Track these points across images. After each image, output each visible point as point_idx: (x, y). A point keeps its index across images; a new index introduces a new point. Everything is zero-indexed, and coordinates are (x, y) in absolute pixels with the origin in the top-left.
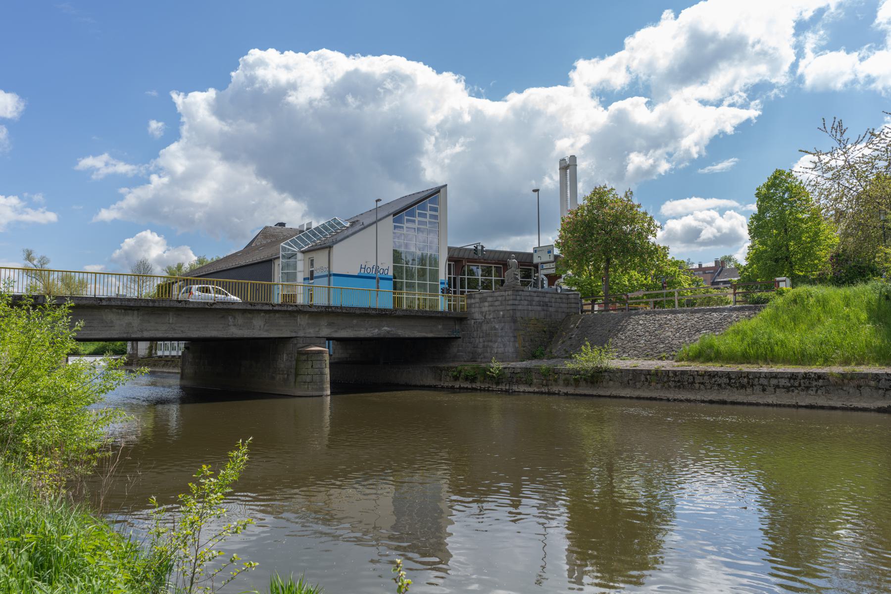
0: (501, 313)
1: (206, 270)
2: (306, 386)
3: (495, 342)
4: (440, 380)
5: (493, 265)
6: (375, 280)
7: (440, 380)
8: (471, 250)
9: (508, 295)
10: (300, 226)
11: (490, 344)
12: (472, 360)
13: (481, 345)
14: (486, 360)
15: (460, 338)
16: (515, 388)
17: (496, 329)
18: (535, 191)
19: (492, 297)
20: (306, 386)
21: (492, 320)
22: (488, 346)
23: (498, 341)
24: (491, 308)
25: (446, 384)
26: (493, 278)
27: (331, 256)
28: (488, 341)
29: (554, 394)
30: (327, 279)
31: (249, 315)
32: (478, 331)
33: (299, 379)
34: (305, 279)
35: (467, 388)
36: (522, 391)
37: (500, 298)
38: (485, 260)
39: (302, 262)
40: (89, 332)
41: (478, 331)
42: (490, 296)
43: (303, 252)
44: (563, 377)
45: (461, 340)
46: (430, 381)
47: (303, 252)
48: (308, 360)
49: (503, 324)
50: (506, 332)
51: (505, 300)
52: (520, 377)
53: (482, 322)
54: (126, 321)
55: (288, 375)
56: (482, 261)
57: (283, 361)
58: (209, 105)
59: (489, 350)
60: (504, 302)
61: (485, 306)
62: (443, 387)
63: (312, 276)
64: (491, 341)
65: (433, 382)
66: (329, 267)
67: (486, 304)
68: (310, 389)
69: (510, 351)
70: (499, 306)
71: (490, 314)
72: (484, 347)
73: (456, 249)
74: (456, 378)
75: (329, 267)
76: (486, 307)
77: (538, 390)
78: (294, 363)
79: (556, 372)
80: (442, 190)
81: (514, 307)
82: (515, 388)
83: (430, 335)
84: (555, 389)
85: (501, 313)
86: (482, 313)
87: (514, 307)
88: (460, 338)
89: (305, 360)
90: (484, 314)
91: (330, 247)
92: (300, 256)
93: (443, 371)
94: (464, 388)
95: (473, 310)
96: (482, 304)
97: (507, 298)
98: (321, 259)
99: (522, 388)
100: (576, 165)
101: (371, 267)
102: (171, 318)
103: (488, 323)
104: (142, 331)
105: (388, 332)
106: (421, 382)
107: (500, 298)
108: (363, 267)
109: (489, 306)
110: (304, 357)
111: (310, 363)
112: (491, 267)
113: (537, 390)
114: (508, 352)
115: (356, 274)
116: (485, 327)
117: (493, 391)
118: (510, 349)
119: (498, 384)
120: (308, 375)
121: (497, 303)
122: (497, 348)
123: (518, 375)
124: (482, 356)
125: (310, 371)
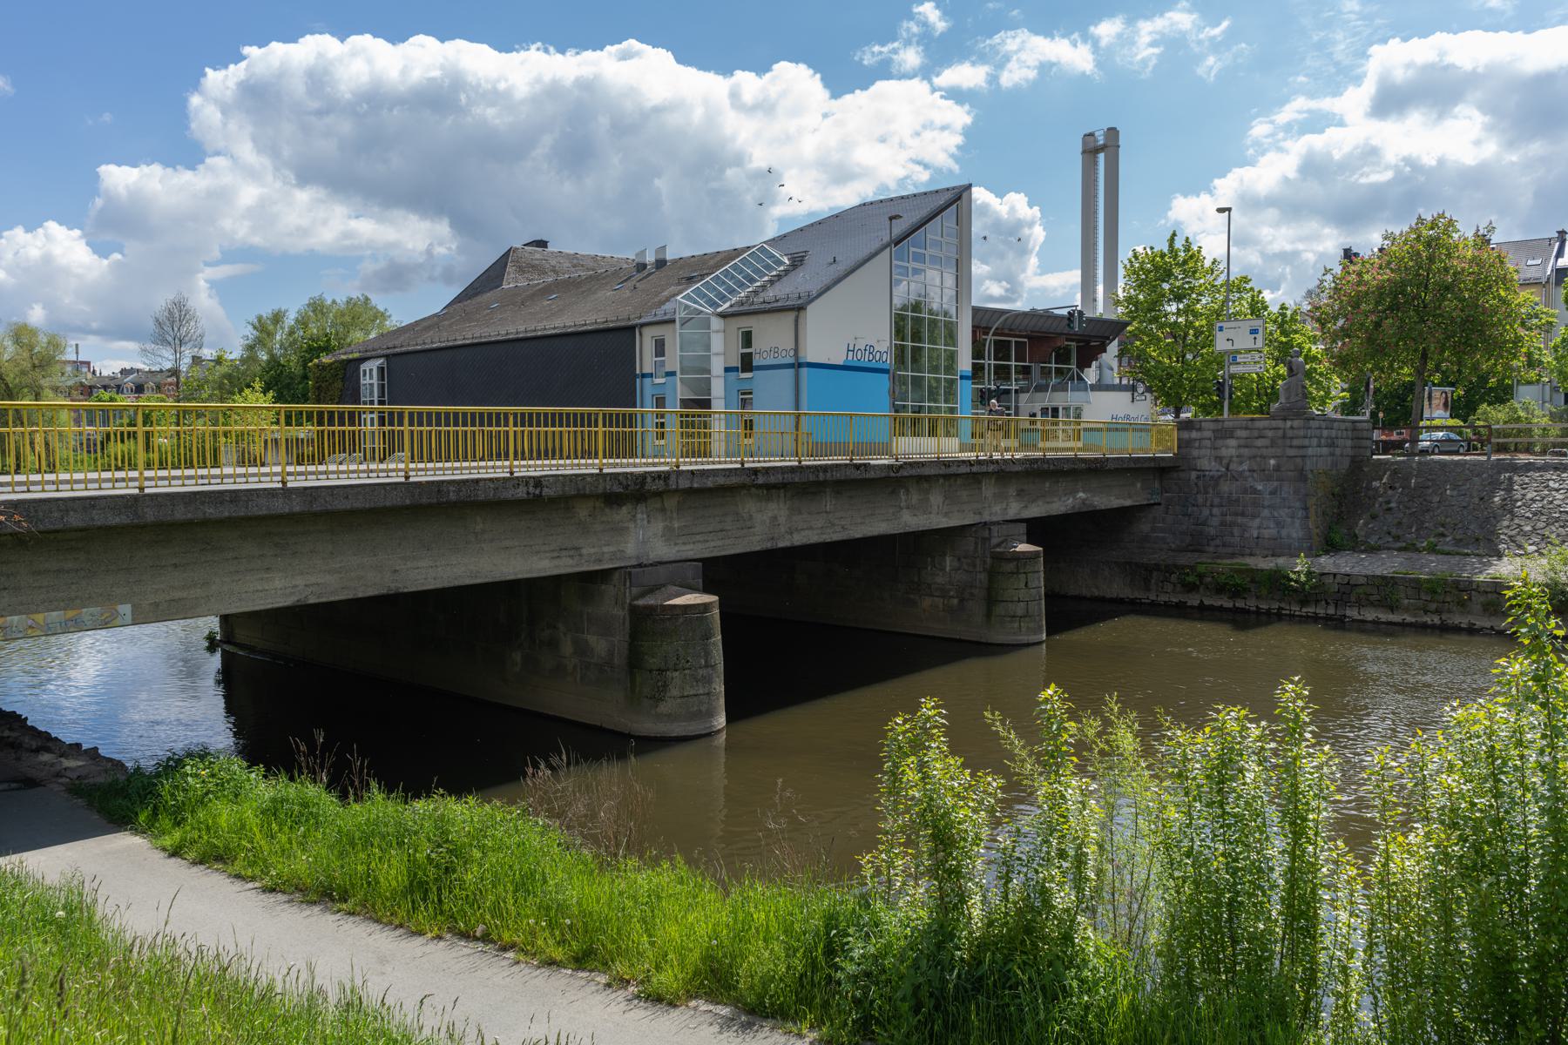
0: (1272, 462)
1: (428, 336)
2: (1016, 625)
3: (1254, 516)
4: (1148, 589)
5: (1013, 339)
6: (887, 376)
7: (1148, 589)
8: (1061, 317)
9: (1292, 428)
10: (637, 255)
11: (1240, 520)
12: (1190, 548)
13: (1215, 521)
14: (1230, 550)
15: (1159, 504)
16: (1352, 613)
17: (1255, 491)
18: (1220, 210)
19: (1246, 428)
20: (1016, 625)
21: (1247, 474)
22: (1232, 524)
23: (1262, 515)
24: (1246, 452)
25: (1163, 598)
26: (1013, 363)
27: (800, 326)
28: (1236, 514)
29: (1457, 629)
30: (791, 372)
31: (926, 485)
32: (1207, 493)
33: (999, 609)
34: (727, 370)
35: (1221, 609)
36: (1370, 619)
37: (1270, 434)
38: (1011, 330)
39: (721, 335)
40: (720, 543)
41: (1207, 493)
42: (1241, 428)
43: (723, 316)
44: (1482, 599)
45: (1161, 508)
46: (1117, 588)
47: (723, 316)
48: (1018, 573)
49: (1275, 484)
50: (1284, 499)
51: (1284, 437)
52: (1365, 594)
53: (1220, 477)
54: (770, 515)
55: (962, 600)
56: (1007, 331)
57: (943, 569)
58: (1442, 116)
59: (1236, 531)
60: (1280, 442)
61: (1227, 447)
62: (1153, 604)
63: (747, 364)
64: (1243, 514)
65: (1127, 593)
66: (796, 350)
67: (1232, 442)
68: (1023, 629)
69: (1294, 535)
70: (1267, 447)
71: (1241, 463)
72: (1223, 524)
73: (987, 310)
74: (1191, 588)
75: (796, 350)
76: (1230, 448)
77: (1413, 620)
78: (983, 577)
79: (1470, 587)
80: (965, 195)
81: (1301, 452)
82: (1352, 613)
83: (1128, 503)
84: (1462, 620)
85: (1272, 462)
86: (1219, 459)
87: (1301, 452)
88: (1159, 504)
89: (1013, 573)
90: (1225, 462)
91: (800, 309)
92: (716, 323)
93: (1155, 573)
94: (1212, 608)
95: (1195, 453)
96: (1219, 443)
97: (1290, 433)
98: (772, 338)
99: (1370, 615)
100: (1119, 146)
101: (863, 348)
102: (828, 502)
103: (1234, 478)
104: (791, 533)
105: (1084, 501)
106: (1095, 590)
107: (1270, 434)
108: (851, 348)
109: (1239, 446)
110: (1011, 567)
111: (1022, 577)
112: (1009, 341)
113: (1409, 619)
114: (1289, 537)
115: (841, 363)
116: (1225, 487)
117: (1292, 616)
118: (1295, 532)
119: (1304, 603)
120: (1019, 601)
121: (1259, 443)
122: (1259, 528)
123: (1360, 590)
124: (1218, 542)
125: (1022, 594)
